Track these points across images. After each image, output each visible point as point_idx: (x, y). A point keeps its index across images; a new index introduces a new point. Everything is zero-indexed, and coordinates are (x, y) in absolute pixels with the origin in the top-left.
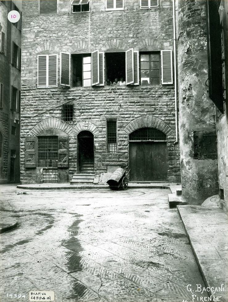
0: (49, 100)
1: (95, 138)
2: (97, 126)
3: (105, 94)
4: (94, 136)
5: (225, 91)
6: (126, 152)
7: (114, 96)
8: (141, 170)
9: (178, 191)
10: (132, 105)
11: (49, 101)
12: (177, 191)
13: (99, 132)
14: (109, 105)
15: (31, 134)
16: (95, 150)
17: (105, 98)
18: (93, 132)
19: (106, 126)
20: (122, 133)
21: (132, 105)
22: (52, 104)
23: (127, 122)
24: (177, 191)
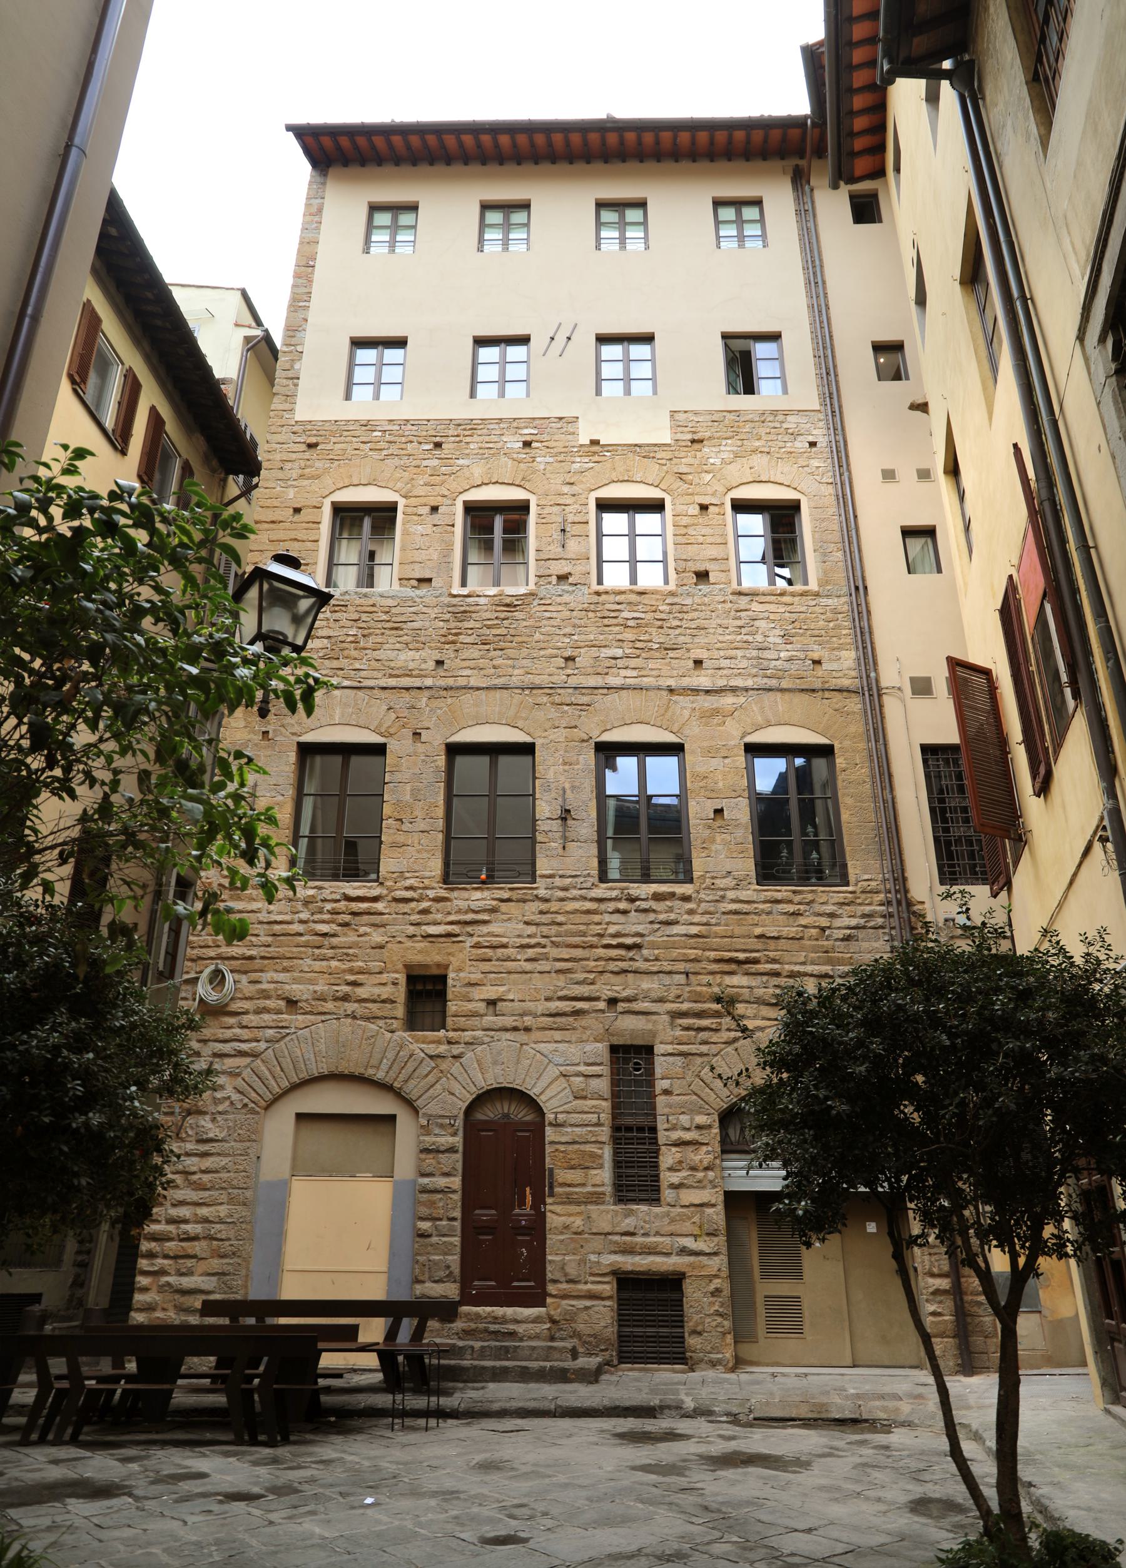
0: (334, 935)
1: (551, 1124)
2: (562, 1069)
3: (597, 918)
4: (550, 1117)
5: (226, 1321)
6: (705, 1200)
7: (640, 928)
8: (857, 1152)
9: (874, 222)
10: (281, 922)
11: (335, 941)
12: (880, 221)
13: (571, 1098)
14: (616, 969)
15: (235, 1097)
16: (551, 1187)
17: (601, 936)
18: (543, 1098)
19: (604, 1070)
20: (688, 1099)
21: (281, 922)
22: (347, 955)
23: (704, 1049)
24: (880, 221)
